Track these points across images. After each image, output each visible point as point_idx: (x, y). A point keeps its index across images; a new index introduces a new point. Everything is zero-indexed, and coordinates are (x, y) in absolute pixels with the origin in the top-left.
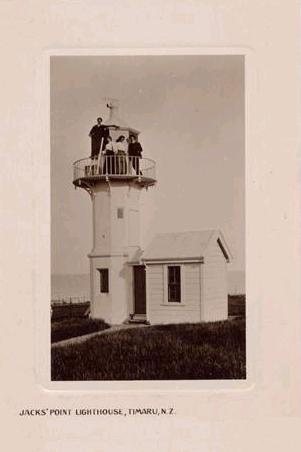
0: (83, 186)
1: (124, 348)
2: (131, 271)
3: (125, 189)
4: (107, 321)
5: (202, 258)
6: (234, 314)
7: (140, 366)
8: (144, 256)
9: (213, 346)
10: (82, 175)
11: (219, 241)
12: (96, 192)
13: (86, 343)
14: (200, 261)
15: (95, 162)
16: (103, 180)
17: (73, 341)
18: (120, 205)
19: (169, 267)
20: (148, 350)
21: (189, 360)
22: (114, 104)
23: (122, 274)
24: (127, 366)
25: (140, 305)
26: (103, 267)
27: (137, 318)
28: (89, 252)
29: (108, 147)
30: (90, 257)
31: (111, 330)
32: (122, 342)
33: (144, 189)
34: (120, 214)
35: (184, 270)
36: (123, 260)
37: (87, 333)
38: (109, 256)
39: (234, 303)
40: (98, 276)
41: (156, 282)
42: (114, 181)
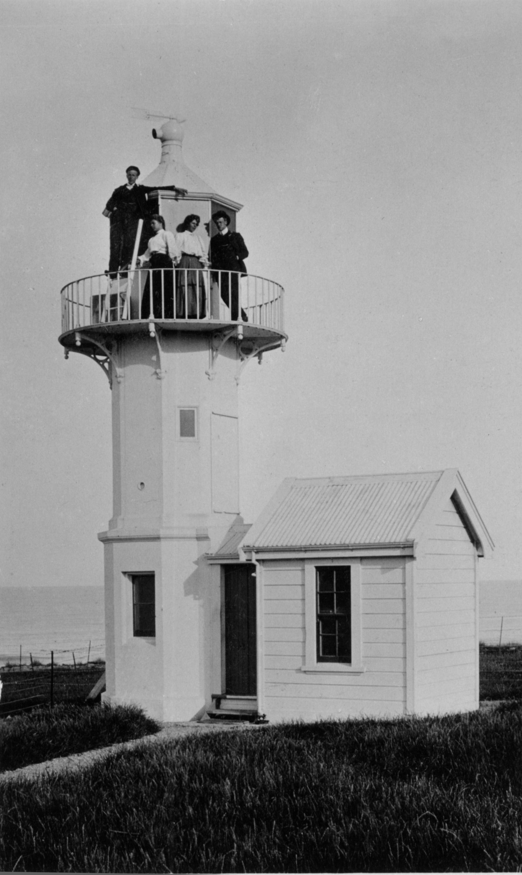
0: (88, 349)
1: (196, 785)
2: (216, 577)
3: (199, 357)
4: (150, 714)
5: (410, 546)
6: (494, 697)
7: (241, 834)
8: (249, 540)
9: (438, 783)
10: (85, 319)
11: (455, 499)
12: (123, 365)
13: (95, 773)
14: (403, 554)
15: (119, 286)
16: (141, 335)
17: (57, 765)
18: (187, 403)
19: (318, 568)
20: (263, 790)
21: (373, 820)
22: (174, 130)
23: (192, 586)
24: (203, 835)
25: (239, 668)
26: (141, 567)
27: (233, 705)
28: (104, 527)
29: (156, 244)
30: (106, 540)
31: (161, 736)
32: (192, 773)
33: (252, 360)
34: (187, 425)
35: (359, 575)
36: (195, 551)
37: (94, 746)
38: (157, 538)
39: (496, 666)
40: (126, 590)
41: (285, 609)
42: (168, 334)
